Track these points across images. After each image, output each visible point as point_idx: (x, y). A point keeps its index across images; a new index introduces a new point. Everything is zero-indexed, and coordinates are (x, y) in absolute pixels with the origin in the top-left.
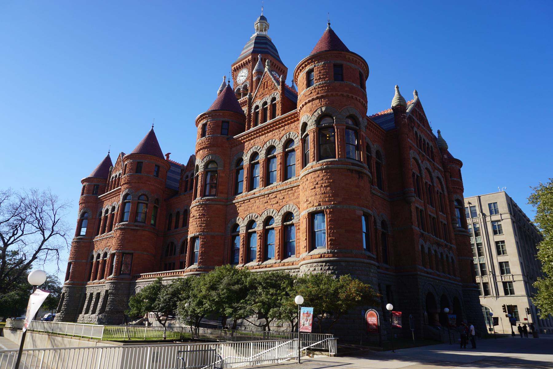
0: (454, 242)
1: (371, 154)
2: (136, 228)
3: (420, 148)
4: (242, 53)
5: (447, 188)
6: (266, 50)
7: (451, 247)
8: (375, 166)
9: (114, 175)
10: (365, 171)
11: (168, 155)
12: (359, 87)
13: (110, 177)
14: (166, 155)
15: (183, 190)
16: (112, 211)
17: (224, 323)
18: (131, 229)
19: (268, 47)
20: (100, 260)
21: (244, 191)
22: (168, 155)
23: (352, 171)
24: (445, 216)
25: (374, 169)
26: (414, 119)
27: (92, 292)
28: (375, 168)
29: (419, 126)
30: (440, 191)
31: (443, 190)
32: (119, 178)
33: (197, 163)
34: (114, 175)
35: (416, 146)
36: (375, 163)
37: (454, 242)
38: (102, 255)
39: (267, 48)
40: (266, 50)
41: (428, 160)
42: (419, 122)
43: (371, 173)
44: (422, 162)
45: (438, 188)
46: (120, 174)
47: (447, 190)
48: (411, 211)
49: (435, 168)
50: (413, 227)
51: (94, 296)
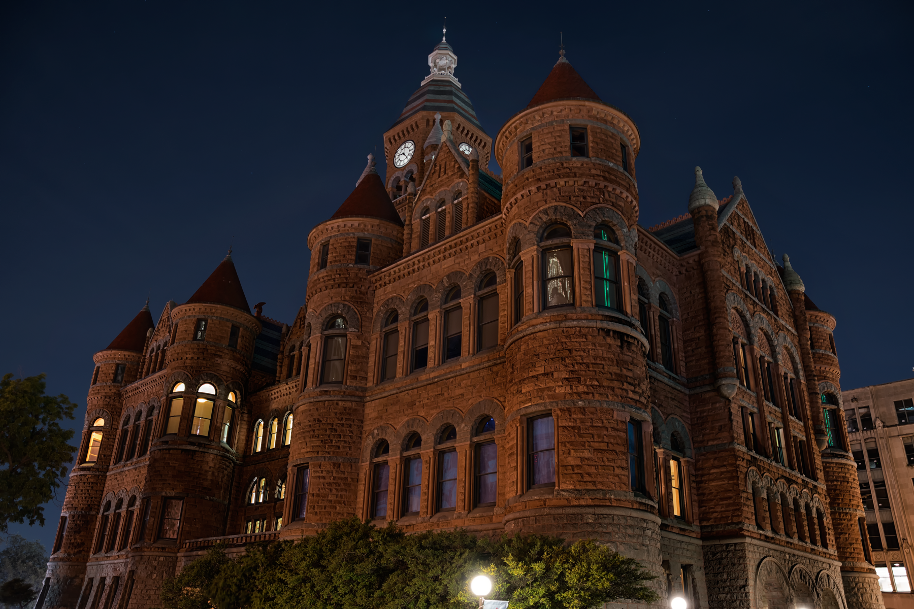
0: (820, 475)
1: (648, 299)
2: (192, 448)
3: (749, 289)
4: (404, 111)
5: (806, 368)
6: (449, 105)
7: (815, 487)
8: (657, 323)
9: (154, 345)
10: (634, 333)
11: (259, 306)
12: (621, 170)
13: (147, 348)
14: (256, 307)
15: (285, 373)
16: (148, 416)
17: (564, 563)
18: (183, 450)
19: (454, 99)
20: (123, 511)
21: (399, 375)
22: (259, 306)
23: (607, 332)
24: (802, 424)
25: (656, 330)
26: (734, 233)
27: (103, 575)
28: (657, 328)
29: (743, 244)
30: (791, 375)
31: (796, 372)
32: (164, 352)
33: (782, 371)
34: (154, 345)
35: (738, 284)
36: (657, 318)
37: (820, 475)
38: (113, 504)
39: (452, 102)
40: (449, 105)
41: (764, 311)
42: (744, 239)
43: (648, 335)
44: (753, 315)
45: (785, 367)
46: (165, 345)
47: (805, 371)
48: (730, 414)
49: (781, 328)
50: (737, 447)
51: (96, 583)
